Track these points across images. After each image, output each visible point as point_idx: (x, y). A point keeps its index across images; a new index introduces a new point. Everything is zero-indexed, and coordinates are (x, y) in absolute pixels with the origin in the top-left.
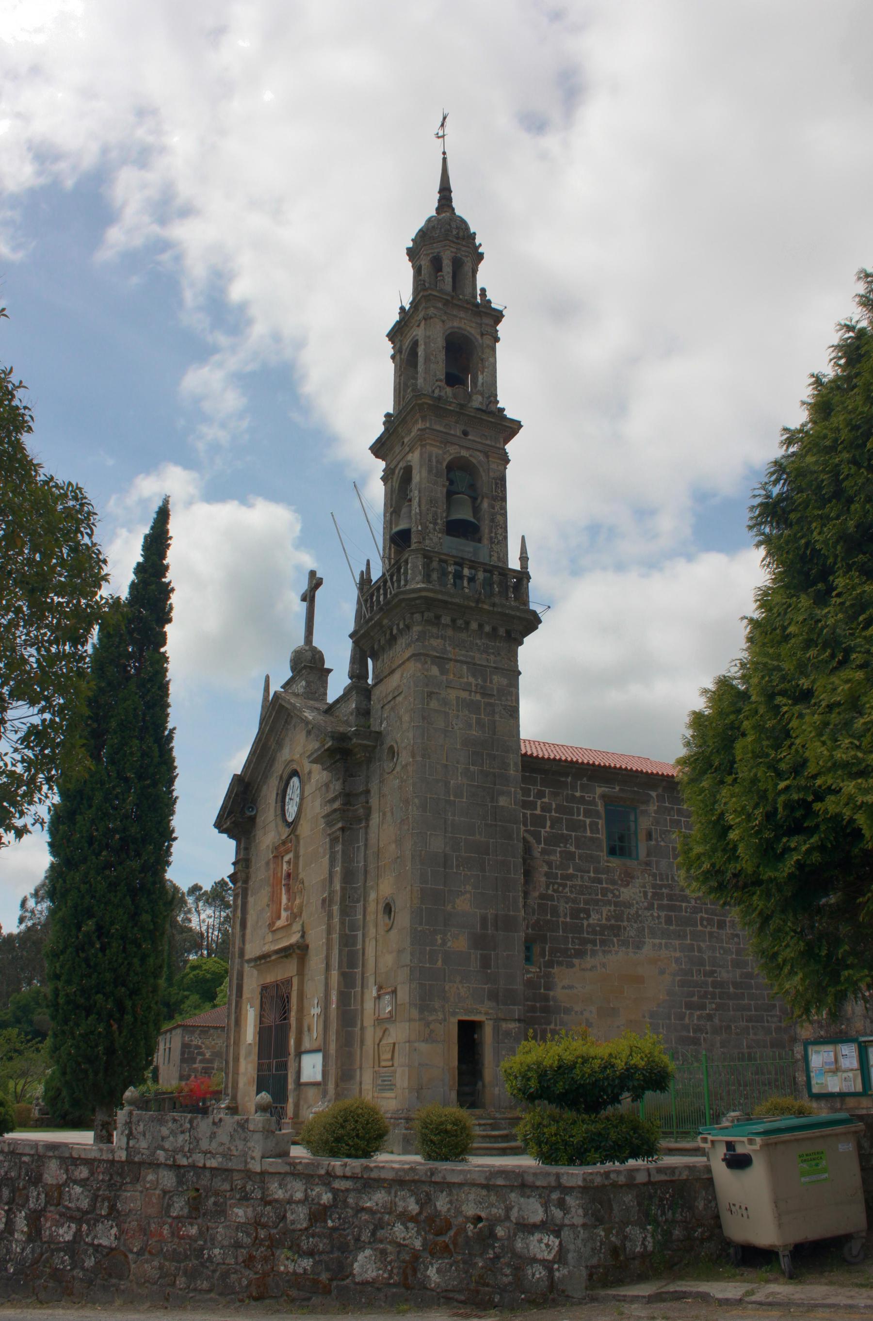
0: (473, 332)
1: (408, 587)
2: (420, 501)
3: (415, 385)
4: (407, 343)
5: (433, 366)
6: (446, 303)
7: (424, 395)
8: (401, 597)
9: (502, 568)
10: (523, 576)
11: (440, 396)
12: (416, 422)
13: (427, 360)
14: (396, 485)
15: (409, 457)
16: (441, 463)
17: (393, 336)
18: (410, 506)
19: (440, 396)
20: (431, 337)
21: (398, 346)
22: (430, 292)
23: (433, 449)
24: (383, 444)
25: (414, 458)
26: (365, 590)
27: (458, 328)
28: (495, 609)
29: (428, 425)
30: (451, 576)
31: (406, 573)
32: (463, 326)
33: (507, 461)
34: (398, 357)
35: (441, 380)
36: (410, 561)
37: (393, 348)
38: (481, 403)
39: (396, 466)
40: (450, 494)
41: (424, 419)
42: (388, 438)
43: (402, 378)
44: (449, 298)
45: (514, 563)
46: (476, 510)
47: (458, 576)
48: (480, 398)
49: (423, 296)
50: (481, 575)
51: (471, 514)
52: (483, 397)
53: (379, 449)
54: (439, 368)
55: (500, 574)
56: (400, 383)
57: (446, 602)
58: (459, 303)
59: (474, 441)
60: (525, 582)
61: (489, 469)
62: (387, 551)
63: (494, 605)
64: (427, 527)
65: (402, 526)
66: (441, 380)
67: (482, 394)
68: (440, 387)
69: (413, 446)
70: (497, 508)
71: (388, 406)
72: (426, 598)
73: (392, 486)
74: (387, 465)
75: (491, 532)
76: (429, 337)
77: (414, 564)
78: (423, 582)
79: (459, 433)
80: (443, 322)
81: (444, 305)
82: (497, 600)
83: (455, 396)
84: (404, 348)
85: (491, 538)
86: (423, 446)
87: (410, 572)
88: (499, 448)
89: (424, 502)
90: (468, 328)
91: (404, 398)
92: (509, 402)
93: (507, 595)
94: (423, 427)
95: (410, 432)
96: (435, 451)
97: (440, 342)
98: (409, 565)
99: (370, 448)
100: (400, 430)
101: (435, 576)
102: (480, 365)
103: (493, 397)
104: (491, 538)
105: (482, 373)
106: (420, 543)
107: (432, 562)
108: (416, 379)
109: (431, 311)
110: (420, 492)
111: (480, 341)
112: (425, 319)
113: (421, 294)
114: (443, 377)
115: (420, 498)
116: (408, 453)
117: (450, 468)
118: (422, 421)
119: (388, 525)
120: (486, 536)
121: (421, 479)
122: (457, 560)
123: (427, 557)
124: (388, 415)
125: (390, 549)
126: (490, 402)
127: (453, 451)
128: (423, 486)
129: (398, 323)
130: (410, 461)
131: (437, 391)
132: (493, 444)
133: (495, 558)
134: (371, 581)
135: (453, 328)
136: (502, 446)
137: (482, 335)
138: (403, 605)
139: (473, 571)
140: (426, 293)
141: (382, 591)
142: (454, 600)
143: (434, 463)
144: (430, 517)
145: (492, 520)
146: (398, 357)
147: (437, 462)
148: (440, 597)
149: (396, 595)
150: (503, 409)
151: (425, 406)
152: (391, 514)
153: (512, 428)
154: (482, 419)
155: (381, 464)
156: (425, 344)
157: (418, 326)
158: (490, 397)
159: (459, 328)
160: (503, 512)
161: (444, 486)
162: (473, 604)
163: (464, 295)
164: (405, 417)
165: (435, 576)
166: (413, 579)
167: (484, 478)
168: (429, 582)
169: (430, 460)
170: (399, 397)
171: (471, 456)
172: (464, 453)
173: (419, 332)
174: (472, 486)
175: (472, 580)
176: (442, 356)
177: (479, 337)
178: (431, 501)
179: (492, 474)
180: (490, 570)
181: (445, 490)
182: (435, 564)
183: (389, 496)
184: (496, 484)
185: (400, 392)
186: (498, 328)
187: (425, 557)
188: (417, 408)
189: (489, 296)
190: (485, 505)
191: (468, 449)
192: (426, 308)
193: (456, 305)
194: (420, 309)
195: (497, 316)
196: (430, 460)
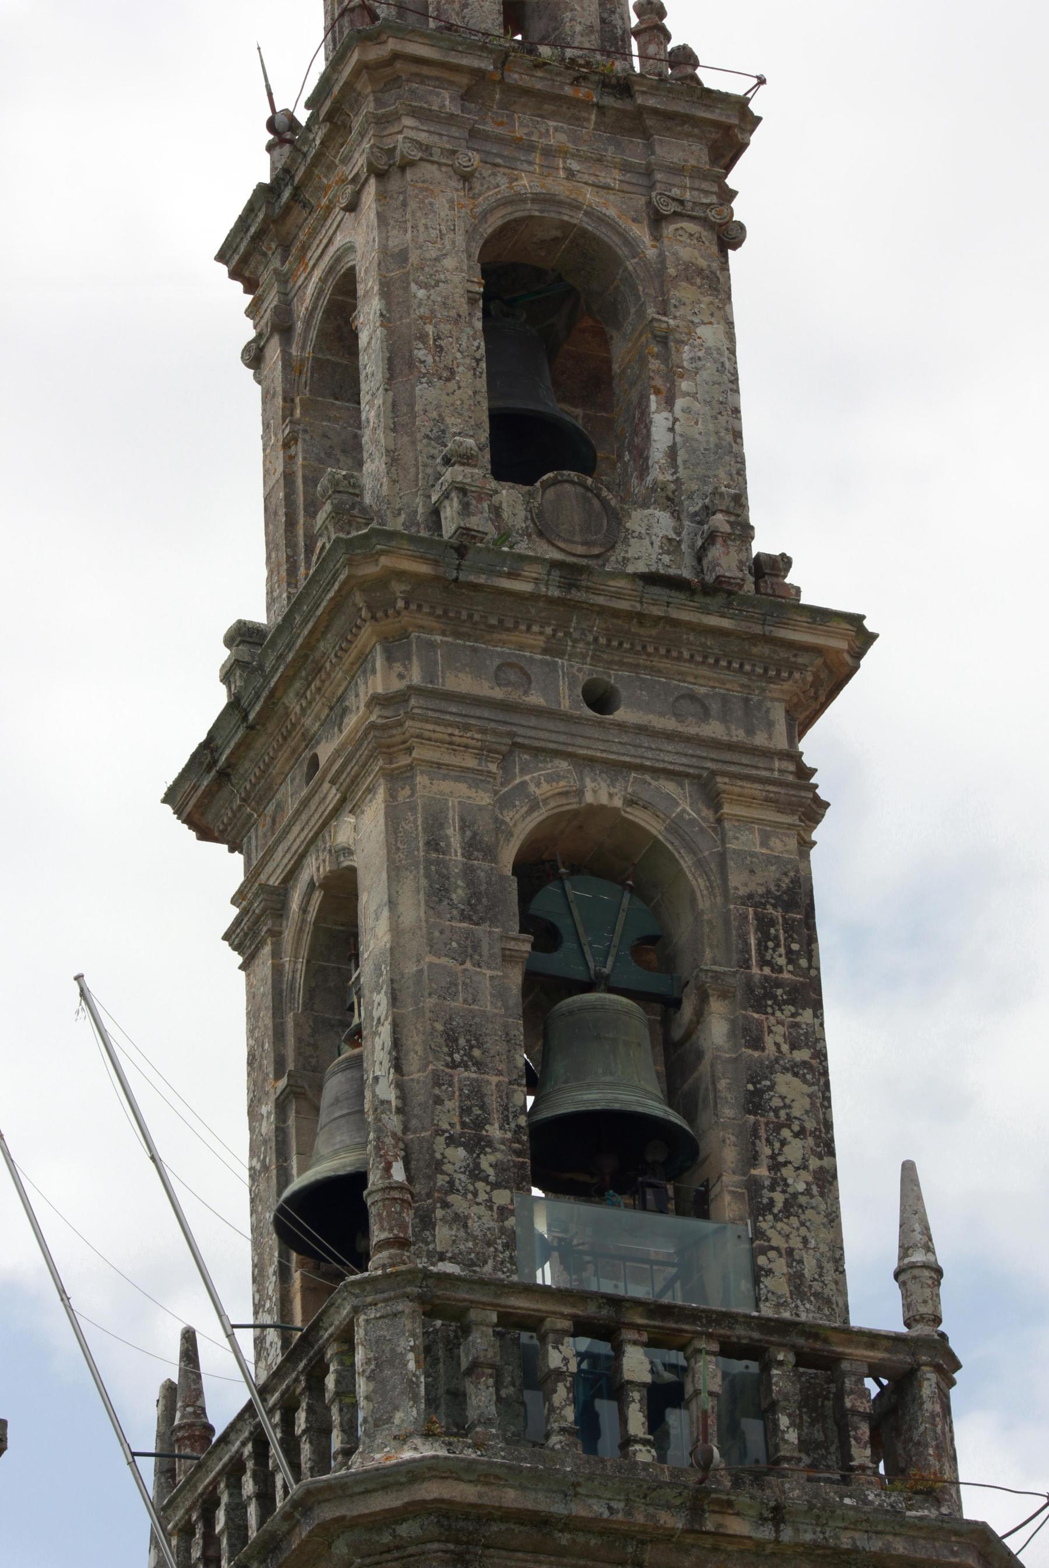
0: (612, 212)
1: (357, 1464)
2: (397, 1043)
3: (355, 489)
4: (310, 289)
5: (427, 394)
6: (475, 88)
7: (392, 535)
8: (327, 1513)
9: (811, 1332)
10: (920, 1364)
11: (465, 532)
12: (363, 664)
13: (399, 363)
14: (296, 968)
15: (344, 833)
16: (490, 853)
17: (257, 247)
18: (357, 1063)
19: (465, 532)
20: (412, 251)
21: (272, 300)
22: (392, 45)
23: (446, 786)
24: (224, 775)
25: (364, 834)
26: (183, 1470)
27: (537, 199)
28: (787, 1534)
29: (416, 677)
30: (561, 1393)
31: (346, 1389)
32: (559, 186)
33: (815, 809)
34: (274, 353)
35: (466, 459)
36: (359, 1334)
37: (252, 312)
38: (672, 545)
39: (291, 875)
40: (543, 993)
41: (396, 647)
42: (244, 745)
43: (299, 450)
44: (487, 65)
45: (874, 1304)
46: (678, 1059)
47: (601, 1382)
48: (663, 522)
49: (364, 66)
50: (709, 1374)
51: (655, 1087)
52: (677, 515)
53: (212, 794)
54: (459, 401)
55: (803, 1359)
56: (288, 477)
57: (542, 1522)
58: (537, 82)
59: (641, 730)
60: (928, 1386)
61: (722, 858)
62: (272, 1283)
63: (777, 1515)
64: (438, 1166)
65: (327, 1165)
66: (466, 459)
67: (672, 503)
68: (463, 491)
69: (354, 781)
70: (774, 1040)
71: (243, 587)
72: (444, 1512)
73: (277, 971)
74: (252, 874)
75: (753, 1159)
76: (402, 256)
77: (384, 1341)
78: (428, 1435)
79: (567, 699)
80: (466, 178)
81: (467, 96)
82: (794, 1490)
83: (542, 527)
84: (301, 309)
85: (753, 1187)
86: (397, 778)
87: (362, 1387)
88: (767, 754)
89: (415, 1041)
90: (590, 196)
91: (309, 550)
92: (810, 524)
93: (846, 1456)
94: (397, 685)
95: (339, 710)
96: (457, 794)
97: (457, 276)
98: (360, 1356)
99: (169, 798)
100: (292, 702)
101: (481, 1398)
102: (654, 364)
103: (727, 510)
104: (753, 1187)
105: (669, 402)
106: (402, 1243)
107: (466, 1330)
108: (353, 449)
109: (407, 134)
110: (394, 999)
111: (651, 253)
112: (381, 176)
113: (355, 57)
114: (475, 438)
115: (395, 1026)
116: (336, 812)
117: (534, 869)
118: (390, 659)
119: (271, 1159)
120: (730, 1180)
121: (395, 929)
122: (590, 1310)
123: (443, 1312)
124: (242, 635)
125: (284, 1273)
126: (711, 538)
127: (548, 790)
128: (411, 968)
129: (263, 194)
130: (348, 851)
131: (450, 513)
132: (738, 735)
133: (777, 1284)
134: (211, 1430)
135: (517, 199)
136: (781, 743)
137: (657, 220)
138: (341, 1548)
139: (677, 1357)
140: (376, 53)
141: (249, 1487)
142: (578, 1509)
143: (456, 856)
144: (449, 1115)
145: (755, 1102)
146: (274, 353)
147: (472, 846)
148: (511, 1498)
149: (303, 1505)
150: (783, 563)
151: (398, 588)
152: (281, 1107)
153: (834, 649)
154: (676, 623)
155: (224, 868)
156: (386, 293)
157: (352, 207)
158: (708, 511)
159: (544, 199)
160: (803, 1055)
161: (508, 958)
162: (674, 1521)
163: (560, 43)
164: (309, 645)
165: (481, 1398)
166: (379, 1422)
167: (703, 904)
168: (460, 1427)
169: (434, 844)
170: (291, 543)
171: (630, 802)
172: (600, 792)
173: (357, 237)
174: (654, 946)
175: (665, 1396)
176: (468, 341)
177: (641, 233)
178: (451, 1038)
179: (738, 881)
180: (748, 1343)
181: (515, 978)
182: (481, 1343)
183: (267, 1018)
184: (764, 924)
185: (291, 524)
186: (732, 180)
187: (431, 1309)
188: (359, 599)
189: (681, 30)
190: (717, 1031)
191: (616, 769)
192: (382, 121)
193: (527, 92)
194: (357, 123)
195: (728, 125)
196: (434, 844)
